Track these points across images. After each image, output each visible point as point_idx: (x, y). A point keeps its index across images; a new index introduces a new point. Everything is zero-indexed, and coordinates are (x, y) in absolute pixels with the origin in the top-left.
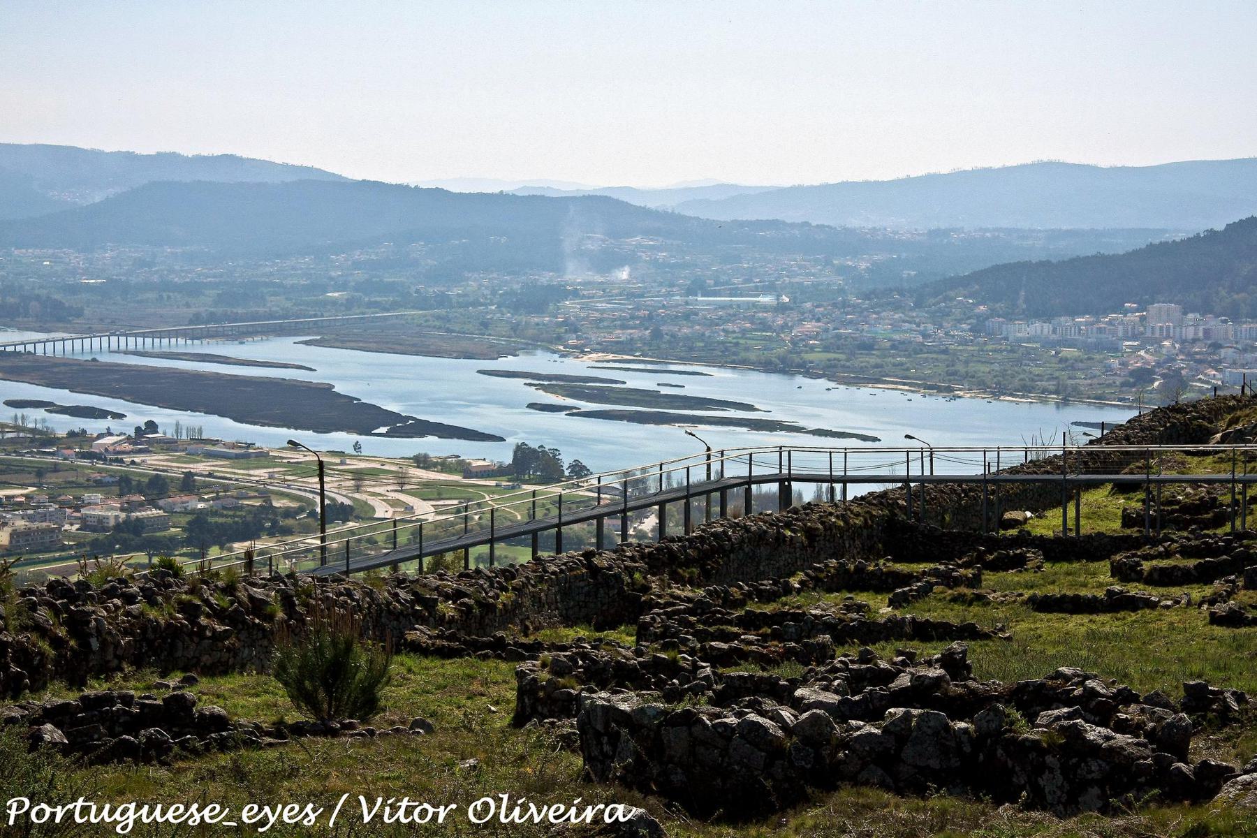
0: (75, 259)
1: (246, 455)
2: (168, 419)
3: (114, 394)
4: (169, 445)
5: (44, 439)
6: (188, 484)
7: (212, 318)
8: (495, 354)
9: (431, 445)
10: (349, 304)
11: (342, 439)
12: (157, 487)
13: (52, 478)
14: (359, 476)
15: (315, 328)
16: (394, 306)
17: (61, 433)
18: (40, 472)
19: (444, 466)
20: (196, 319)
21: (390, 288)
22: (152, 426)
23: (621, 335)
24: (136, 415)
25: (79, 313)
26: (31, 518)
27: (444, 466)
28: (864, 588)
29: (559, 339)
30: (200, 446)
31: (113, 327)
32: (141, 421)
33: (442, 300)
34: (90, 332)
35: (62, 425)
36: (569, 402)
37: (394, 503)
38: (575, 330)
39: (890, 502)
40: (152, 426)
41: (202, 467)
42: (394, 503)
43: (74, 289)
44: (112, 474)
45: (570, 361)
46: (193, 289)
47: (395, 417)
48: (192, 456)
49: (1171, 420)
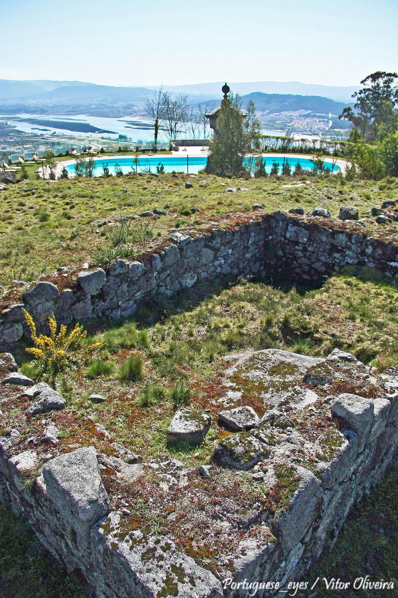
0: (49, 101)
1: (71, 138)
2: (58, 131)
3: (50, 126)
4: (58, 136)
5: (36, 136)
6: (59, 144)
7: (71, 111)
8: (120, 117)
9: (105, 135)
10: (95, 108)
11: (89, 134)
12: (53, 144)
13: (35, 143)
14: (90, 141)
15: (89, 113)
16: (104, 108)
17: (39, 134)
18: (33, 142)
19: (106, 139)
20: (68, 112)
21: (103, 105)
22: (55, 133)
23: (143, 113)
24: (53, 130)
25: (47, 111)
26: (29, 151)
27: (106, 139)
28: (19, 384)
29: (132, 114)
30: (63, 136)
31: (53, 113)
32: (53, 131)
33: (112, 107)
34: (49, 114)
35: (39, 133)
36: (132, 126)
37: (96, 146)
38: (135, 112)
39: (66, 275)
40: (55, 133)
41: (63, 140)
42: (96, 146)
43: (47, 107)
44: (45, 142)
45: (134, 118)
46: (68, 106)
47: (100, 130)
48: (62, 138)
49: (354, 476)
